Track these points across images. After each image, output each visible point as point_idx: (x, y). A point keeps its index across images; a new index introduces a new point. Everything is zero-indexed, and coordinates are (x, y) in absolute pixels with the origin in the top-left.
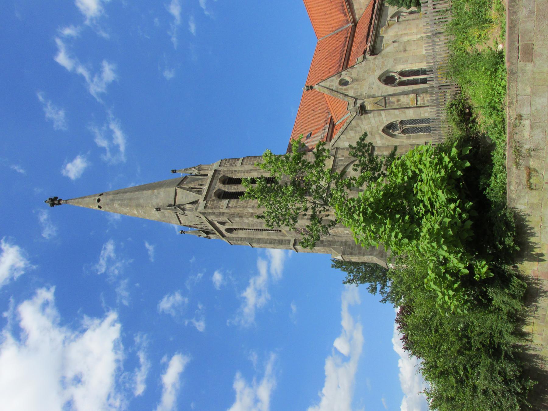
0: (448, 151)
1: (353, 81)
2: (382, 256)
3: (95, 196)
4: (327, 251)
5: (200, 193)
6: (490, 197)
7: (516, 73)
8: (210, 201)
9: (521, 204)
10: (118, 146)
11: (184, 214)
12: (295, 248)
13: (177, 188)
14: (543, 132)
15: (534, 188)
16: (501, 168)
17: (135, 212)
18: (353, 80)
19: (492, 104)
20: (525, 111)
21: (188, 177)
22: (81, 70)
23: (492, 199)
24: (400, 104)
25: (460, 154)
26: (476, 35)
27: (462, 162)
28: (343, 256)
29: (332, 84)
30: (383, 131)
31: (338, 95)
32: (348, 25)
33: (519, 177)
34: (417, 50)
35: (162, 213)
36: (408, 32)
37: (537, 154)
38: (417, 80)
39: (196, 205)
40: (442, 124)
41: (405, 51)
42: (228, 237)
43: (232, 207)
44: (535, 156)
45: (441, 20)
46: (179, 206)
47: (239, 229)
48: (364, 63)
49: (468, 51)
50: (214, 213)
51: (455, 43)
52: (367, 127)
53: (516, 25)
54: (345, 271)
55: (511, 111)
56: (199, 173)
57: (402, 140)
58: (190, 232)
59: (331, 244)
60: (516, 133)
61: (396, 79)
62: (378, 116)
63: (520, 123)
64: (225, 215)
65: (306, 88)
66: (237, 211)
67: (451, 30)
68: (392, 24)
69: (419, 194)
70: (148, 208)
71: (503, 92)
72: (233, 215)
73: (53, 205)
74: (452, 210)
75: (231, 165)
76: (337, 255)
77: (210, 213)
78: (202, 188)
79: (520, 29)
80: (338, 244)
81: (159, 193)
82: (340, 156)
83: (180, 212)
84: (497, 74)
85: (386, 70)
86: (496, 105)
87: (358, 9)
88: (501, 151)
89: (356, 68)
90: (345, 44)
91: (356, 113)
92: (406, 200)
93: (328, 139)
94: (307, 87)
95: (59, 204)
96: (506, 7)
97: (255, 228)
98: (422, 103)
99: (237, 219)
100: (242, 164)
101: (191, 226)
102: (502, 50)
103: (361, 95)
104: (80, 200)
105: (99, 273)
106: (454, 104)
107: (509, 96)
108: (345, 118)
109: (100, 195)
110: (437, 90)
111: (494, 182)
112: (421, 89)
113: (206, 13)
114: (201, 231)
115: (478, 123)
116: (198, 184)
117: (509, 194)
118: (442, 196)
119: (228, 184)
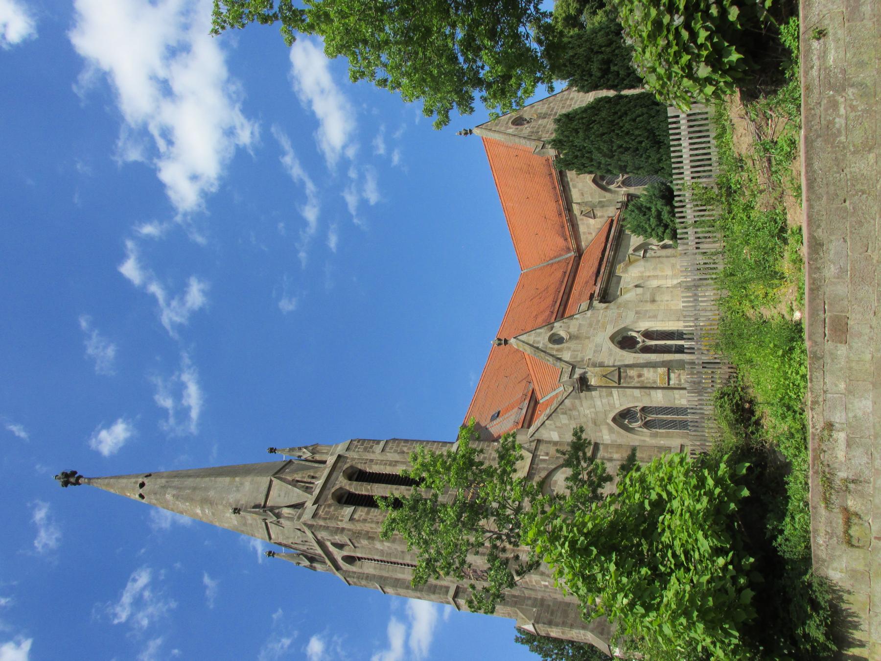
0: (713, 468)
1: (570, 338)
2: (602, 634)
3: (137, 476)
4: (509, 614)
5: (309, 490)
6: (784, 552)
7: (822, 358)
8: (323, 507)
9: (835, 569)
10: (189, 408)
11: (278, 524)
12: (455, 603)
13: (273, 478)
14: (867, 453)
15: (857, 544)
16: (801, 504)
17: (199, 511)
18: (572, 337)
19: (786, 401)
20: (838, 418)
21: (293, 463)
22: (155, 289)
23: (787, 556)
24: (643, 381)
25: (733, 477)
26: (761, 293)
27: (736, 488)
28: (536, 625)
29: (538, 339)
30: (614, 420)
31: (547, 358)
32: (569, 255)
33: (831, 523)
34: (672, 302)
35: (242, 517)
36: (660, 274)
37: (860, 488)
38: (671, 346)
39: (300, 511)
40: (706, 422)
41: (653, 301)
42: (346, 571)
43: (358, 521)
44: (856, 491)
45: (707, 266)
46: (272, 509)
47: (365, 559)
48: (589, 313)
49: (748, 315)
50: (328, 527)
51: (728, 302)
52: (588, 412)
53: (820, 286)
54: (536, 651)
55: (815, 416)
56: (313, 458)
57: (643, 438)
58: (283, 556)
59: (517, 602)
60: (825, 451)
61: (638, 342)
62: (607, 396)
63: (831, 436)
64: (346, 532)
65: (497, 342)
66: (367, 527)
67: (722, 281)
68: (636, 261)
69: (667, 533)
70: (220, 507)
71: (802, 384)
72: (358, 533)
73: (66, 484)
74: (720, 568)
75: (365, 449)
76: (526, 623)
77: (321, 526)
78: (313, 483)
79: (827, 293)
80: (530, 602)
81: (242, 484)
82: (542, 453)
83: (272, 518)
84: (793, 356)
85: (623, 326)
86: (792, 403)
87: (584, 233)
88: (801, 478)
89: (577, 319)
90: (562, 282)
91: (572, 388)
92: (646, 540)
93: (526, 425)
94: (499, 339)
95: (77, 483)
96: (805, 260)
97: (393, 560)
98: (677, 382)
99: (365, 542)
100: (383, 451)
101: (285, 546)
102: (800, 320)
103: (583, 361)
104: (112, 481)
105: (116, 621)
106: (727, 393)
107: (812, 392)
108: (554, 393)
109: (147, 476)
110: (699, 368)
111: (789, 526)
112: (676, 361)
113: (355, 221)
114: (301, 556)
115: (765, 427)
116: (309, 476)
117: (814, 550)
118: (705, 545)
119: (356, 480)
